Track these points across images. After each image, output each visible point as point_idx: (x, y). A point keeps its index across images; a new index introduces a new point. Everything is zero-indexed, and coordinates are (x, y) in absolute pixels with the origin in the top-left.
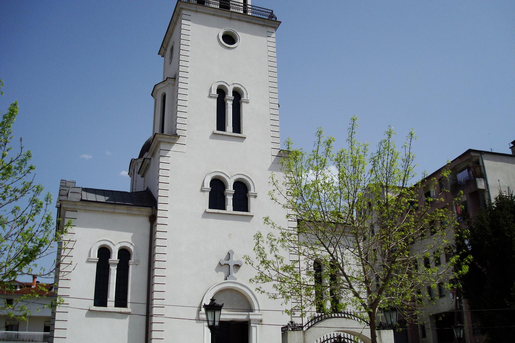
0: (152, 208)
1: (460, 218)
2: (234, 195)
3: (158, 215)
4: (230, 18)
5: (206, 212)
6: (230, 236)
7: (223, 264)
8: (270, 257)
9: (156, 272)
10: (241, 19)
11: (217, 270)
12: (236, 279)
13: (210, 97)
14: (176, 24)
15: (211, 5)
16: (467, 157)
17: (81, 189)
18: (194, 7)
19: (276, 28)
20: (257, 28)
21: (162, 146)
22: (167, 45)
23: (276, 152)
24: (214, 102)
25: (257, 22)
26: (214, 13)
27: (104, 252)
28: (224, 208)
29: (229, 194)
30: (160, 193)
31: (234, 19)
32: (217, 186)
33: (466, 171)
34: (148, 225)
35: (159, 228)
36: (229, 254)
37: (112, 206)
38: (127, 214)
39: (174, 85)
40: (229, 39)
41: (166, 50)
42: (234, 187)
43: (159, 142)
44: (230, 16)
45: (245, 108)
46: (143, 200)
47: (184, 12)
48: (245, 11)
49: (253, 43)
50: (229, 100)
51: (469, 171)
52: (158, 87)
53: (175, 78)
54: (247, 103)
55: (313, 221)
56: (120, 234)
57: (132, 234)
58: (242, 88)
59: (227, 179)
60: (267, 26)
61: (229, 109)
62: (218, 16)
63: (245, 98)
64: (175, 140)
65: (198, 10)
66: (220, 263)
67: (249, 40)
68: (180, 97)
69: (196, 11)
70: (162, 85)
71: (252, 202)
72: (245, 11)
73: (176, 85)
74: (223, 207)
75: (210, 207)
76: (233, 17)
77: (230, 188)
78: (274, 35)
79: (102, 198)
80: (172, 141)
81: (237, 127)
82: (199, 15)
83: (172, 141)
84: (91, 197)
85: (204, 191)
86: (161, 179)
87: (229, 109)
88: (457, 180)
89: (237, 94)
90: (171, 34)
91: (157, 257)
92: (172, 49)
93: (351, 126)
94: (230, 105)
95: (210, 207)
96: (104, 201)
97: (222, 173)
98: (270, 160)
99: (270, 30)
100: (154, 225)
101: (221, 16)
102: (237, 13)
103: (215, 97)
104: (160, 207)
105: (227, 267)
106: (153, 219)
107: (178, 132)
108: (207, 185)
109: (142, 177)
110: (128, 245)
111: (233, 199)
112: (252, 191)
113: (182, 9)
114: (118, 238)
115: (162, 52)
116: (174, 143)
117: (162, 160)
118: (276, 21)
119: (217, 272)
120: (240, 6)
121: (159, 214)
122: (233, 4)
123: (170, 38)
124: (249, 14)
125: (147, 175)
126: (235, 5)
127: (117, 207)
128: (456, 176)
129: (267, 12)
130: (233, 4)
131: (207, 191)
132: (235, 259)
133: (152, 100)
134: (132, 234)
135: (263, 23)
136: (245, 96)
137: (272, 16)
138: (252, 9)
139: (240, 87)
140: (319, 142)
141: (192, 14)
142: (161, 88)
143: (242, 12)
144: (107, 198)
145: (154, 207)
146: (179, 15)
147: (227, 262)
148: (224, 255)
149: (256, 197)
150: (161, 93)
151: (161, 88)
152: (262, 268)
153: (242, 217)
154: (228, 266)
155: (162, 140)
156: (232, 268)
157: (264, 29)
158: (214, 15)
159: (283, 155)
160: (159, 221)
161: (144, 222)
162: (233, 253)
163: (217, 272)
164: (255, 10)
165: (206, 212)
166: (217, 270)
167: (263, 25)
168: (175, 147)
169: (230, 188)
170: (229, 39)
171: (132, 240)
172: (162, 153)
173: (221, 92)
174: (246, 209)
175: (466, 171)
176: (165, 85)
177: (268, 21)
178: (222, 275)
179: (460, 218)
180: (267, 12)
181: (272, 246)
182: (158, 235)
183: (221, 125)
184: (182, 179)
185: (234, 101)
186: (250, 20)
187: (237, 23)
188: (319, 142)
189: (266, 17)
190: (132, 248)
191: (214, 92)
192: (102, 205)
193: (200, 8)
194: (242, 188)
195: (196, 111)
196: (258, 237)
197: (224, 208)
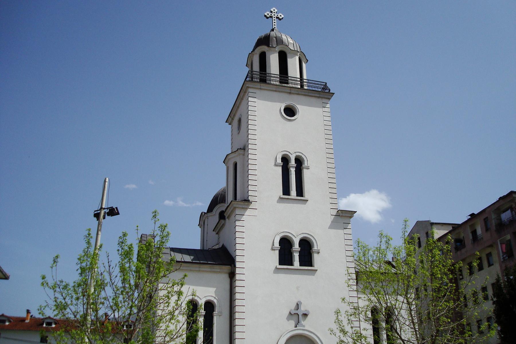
0: (231, 266)
1: (505, 256)
2: (300, 252)
3: (237, 272)
4: (290, 93)
5: (276, 268)
6: (298, 288)
7: (292, 313)
8: (348, 328)
9: (237, 322)
10: (300, 93)
11: (288, 319)
12: (304, 326)
13: (276, 165)
14: (242, 99)
15: (273, 83)
16: (509, 199)
17: (169, 250)
18: (258, 85)
19: (329, 99)
20: (313, 100)
21: (238, 212)
22: (234, 115)
23: (334, 212)
24: (280, 169)
25: (314, 95)
26: (276, 89)
27: (193, 305)
28: (292, 264)
29: (295, 251)
30: (238, 253)
31: (294, 94)
32: (285, 244)
33: (509, 211)
34: (228, 280)
35: (238, 283)
36: (298, 304)
37: (197, 266)
38: (210, 272)
39: (244, 155)
40: (290, 112)
41: (233, 119)
42: (300, 245)
43: (235, 208)
44: (289, 91)
45: (306, 174)
46: (219, 257)
47: (250, 90)
48: (302, 86)
49: (312, 115)
50: (293, 167)
51: (512, 212)
52: (229, 157)
53: (244, 149)
54: (308, 168)
55: (370, 275)
56: (204, 289)
57: (215, 289)
58: (303, 156)
59: (294, 238)
60: (322, 98)
61: (292, 174)
62: (279, 92)
63: (305, 164)
64: (249, 205)
65: (262, 87)
66: (290, 313)
67: (309, 113)
68: (250, 167)
69: (260, 89)
70: (233, 155)
71: (316, 258)
72: (302, 86)
73: (246, 154)
74: (290, 263)
75: (280, 264)
76: (292, 92)
77: (296, 246)
78: (328, 106)
79: (188, 258)
80: (246, 207)
81: (300, 192)
82: (263, 92)
83: (246, 207)
84: (178, 257)
85: (274, 250)
86: (238, 241)
87: (292, 174)
88: (501, 219)
89: (299, 161)
90: (238, 107)
91: (237, 309)
92: (240, 121)
93: (404, 226)
94: (293, 171)
95: (280, 264)
96: (190, 261)
97: (289, 233)
98: (329, 219)
99: (325, 101)
100: (233, 281)
101: (282, 92)
102: (295, 88)
103: (279, 166)
104: (238, 265)
105: (297, 316)
106: (232, 275)
107: (250, 198)
108: (277, 245)
109: (217, 234)
110: (212, 299)
111: (299, 256)
112: (315, 248)
113: (248, 87)
114: (204, 293)
115: (229, 120)
116: (247, 209)
117: (238, 223)
118: (329, 92)
119: (288, 320)
120: (296, 81)
121: (238, 271)
122: (291, 80)
123: (237, 110)
124: (306, 88)
125: (222, 233)
126: (293, 80)
127: (202, 266)
128: (500, 216)
129: (321, 85)
130: (291, 80)
131: (277, 250)
132: (303, 309)
133: (224, 167)
134: (215, 289)
135: (318, 96)
136: (306, 162)
137: (325, 87)
138: (307, 82)
139: (301, 155)
140: (381, 242)
141: (257, 91)
142: (233, 158)
143: (299, 87)
144: (192, 257)
145: (233, 265)
146: (245, 92)
147: (296, 312)
148: (293, 306)
149: (318, 253)
150: (233, 162)
151: (233, 158)
152: (342, 335)
153: (307, 271)
154: (298, 315)
155: (237, 206)
156: (300, 316)
157: (320, 101)
158: (276, 91)
159: (341, 215)
160: (238, 277)
161: (224, 278)
162: (301, 303)
163: (288, 320)
164: (311, 83)
165: (276, 268)
166: (288, 319)
167: (319, 97)
168: (248, 212)
169: (296, 246)
170: (290, 112)
171: (216, 294)
172: (238, 217)
173: (285, 160)
174: (311, 265)
175: (509, 211)
176: (236, 155)
177: (322, 93)
178: (292, 323)
179: (505, 256)
180: (321, 85)
181: (349, 320)
182: (237, 290)
183: (286, 191)
184: (254, 237)
185: (296, 168)
186: (307, 94)
187: (295, 97)
188: (381, 242)
189: (320, 90)
190: (215, 301)
191: (279, 161)
192: (188, 265)
193: (263, 86)
194: (307, 246)
195: (264, 178)
196: (338, 312)
197: (292, 264)
